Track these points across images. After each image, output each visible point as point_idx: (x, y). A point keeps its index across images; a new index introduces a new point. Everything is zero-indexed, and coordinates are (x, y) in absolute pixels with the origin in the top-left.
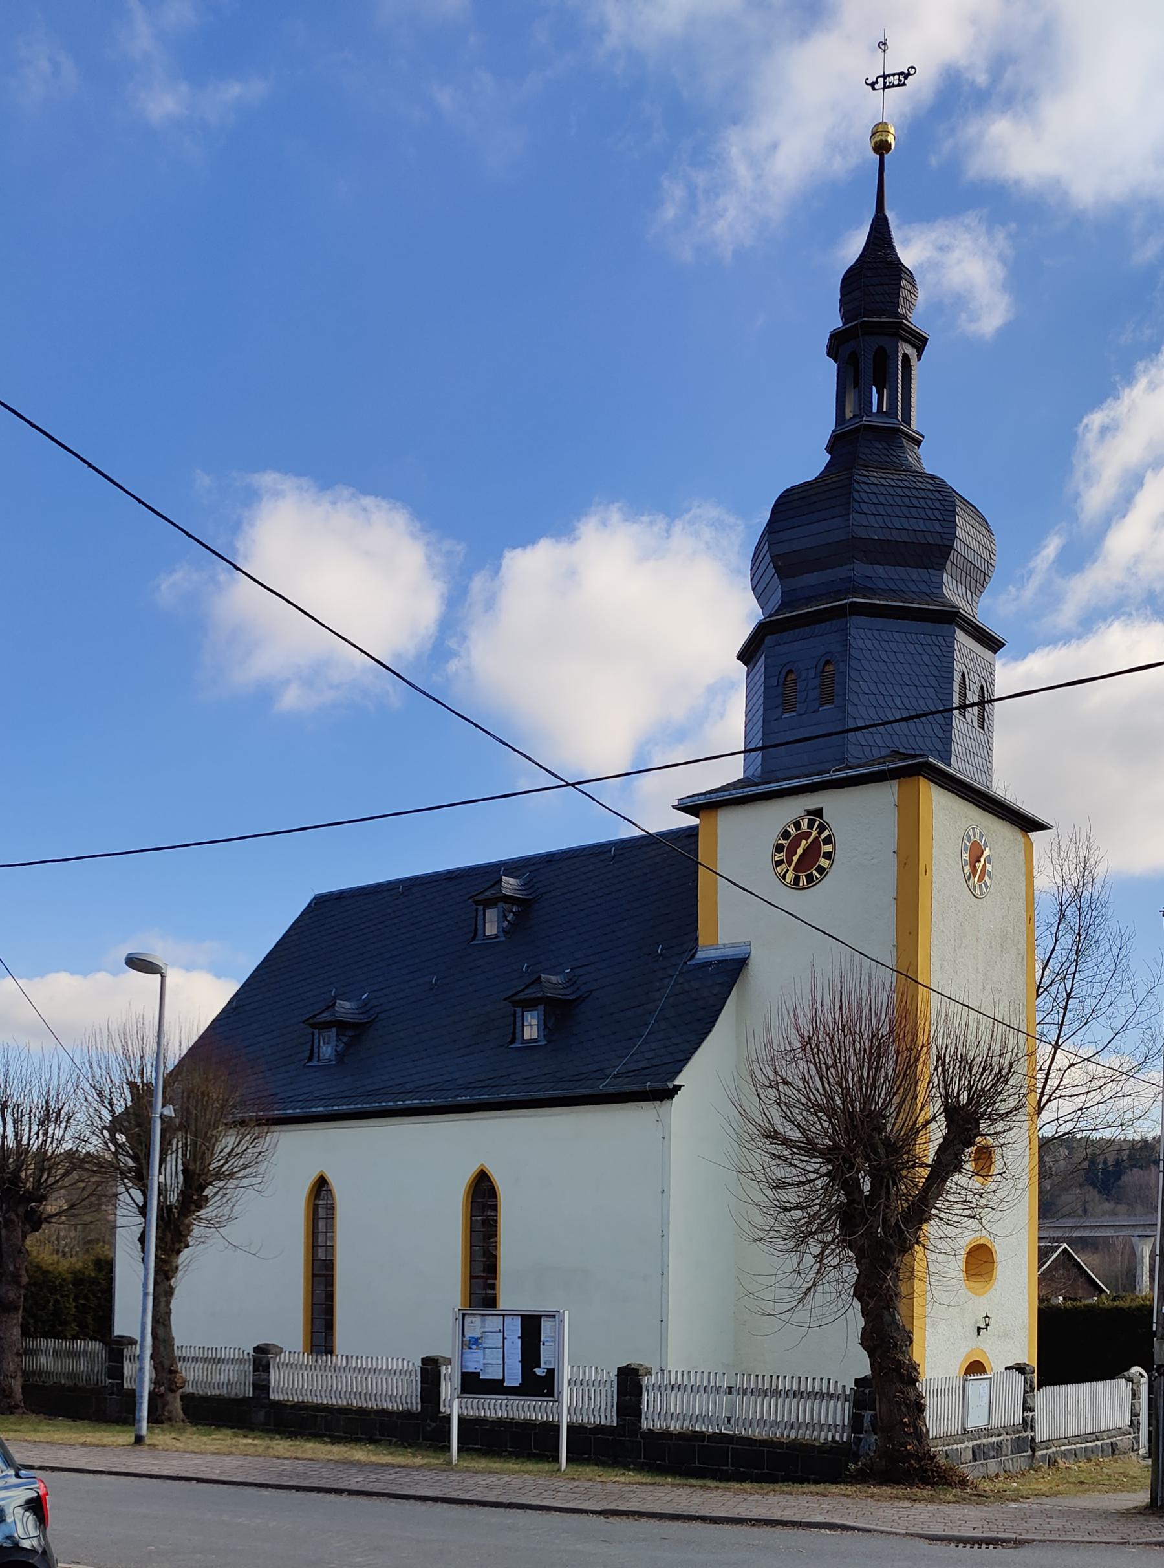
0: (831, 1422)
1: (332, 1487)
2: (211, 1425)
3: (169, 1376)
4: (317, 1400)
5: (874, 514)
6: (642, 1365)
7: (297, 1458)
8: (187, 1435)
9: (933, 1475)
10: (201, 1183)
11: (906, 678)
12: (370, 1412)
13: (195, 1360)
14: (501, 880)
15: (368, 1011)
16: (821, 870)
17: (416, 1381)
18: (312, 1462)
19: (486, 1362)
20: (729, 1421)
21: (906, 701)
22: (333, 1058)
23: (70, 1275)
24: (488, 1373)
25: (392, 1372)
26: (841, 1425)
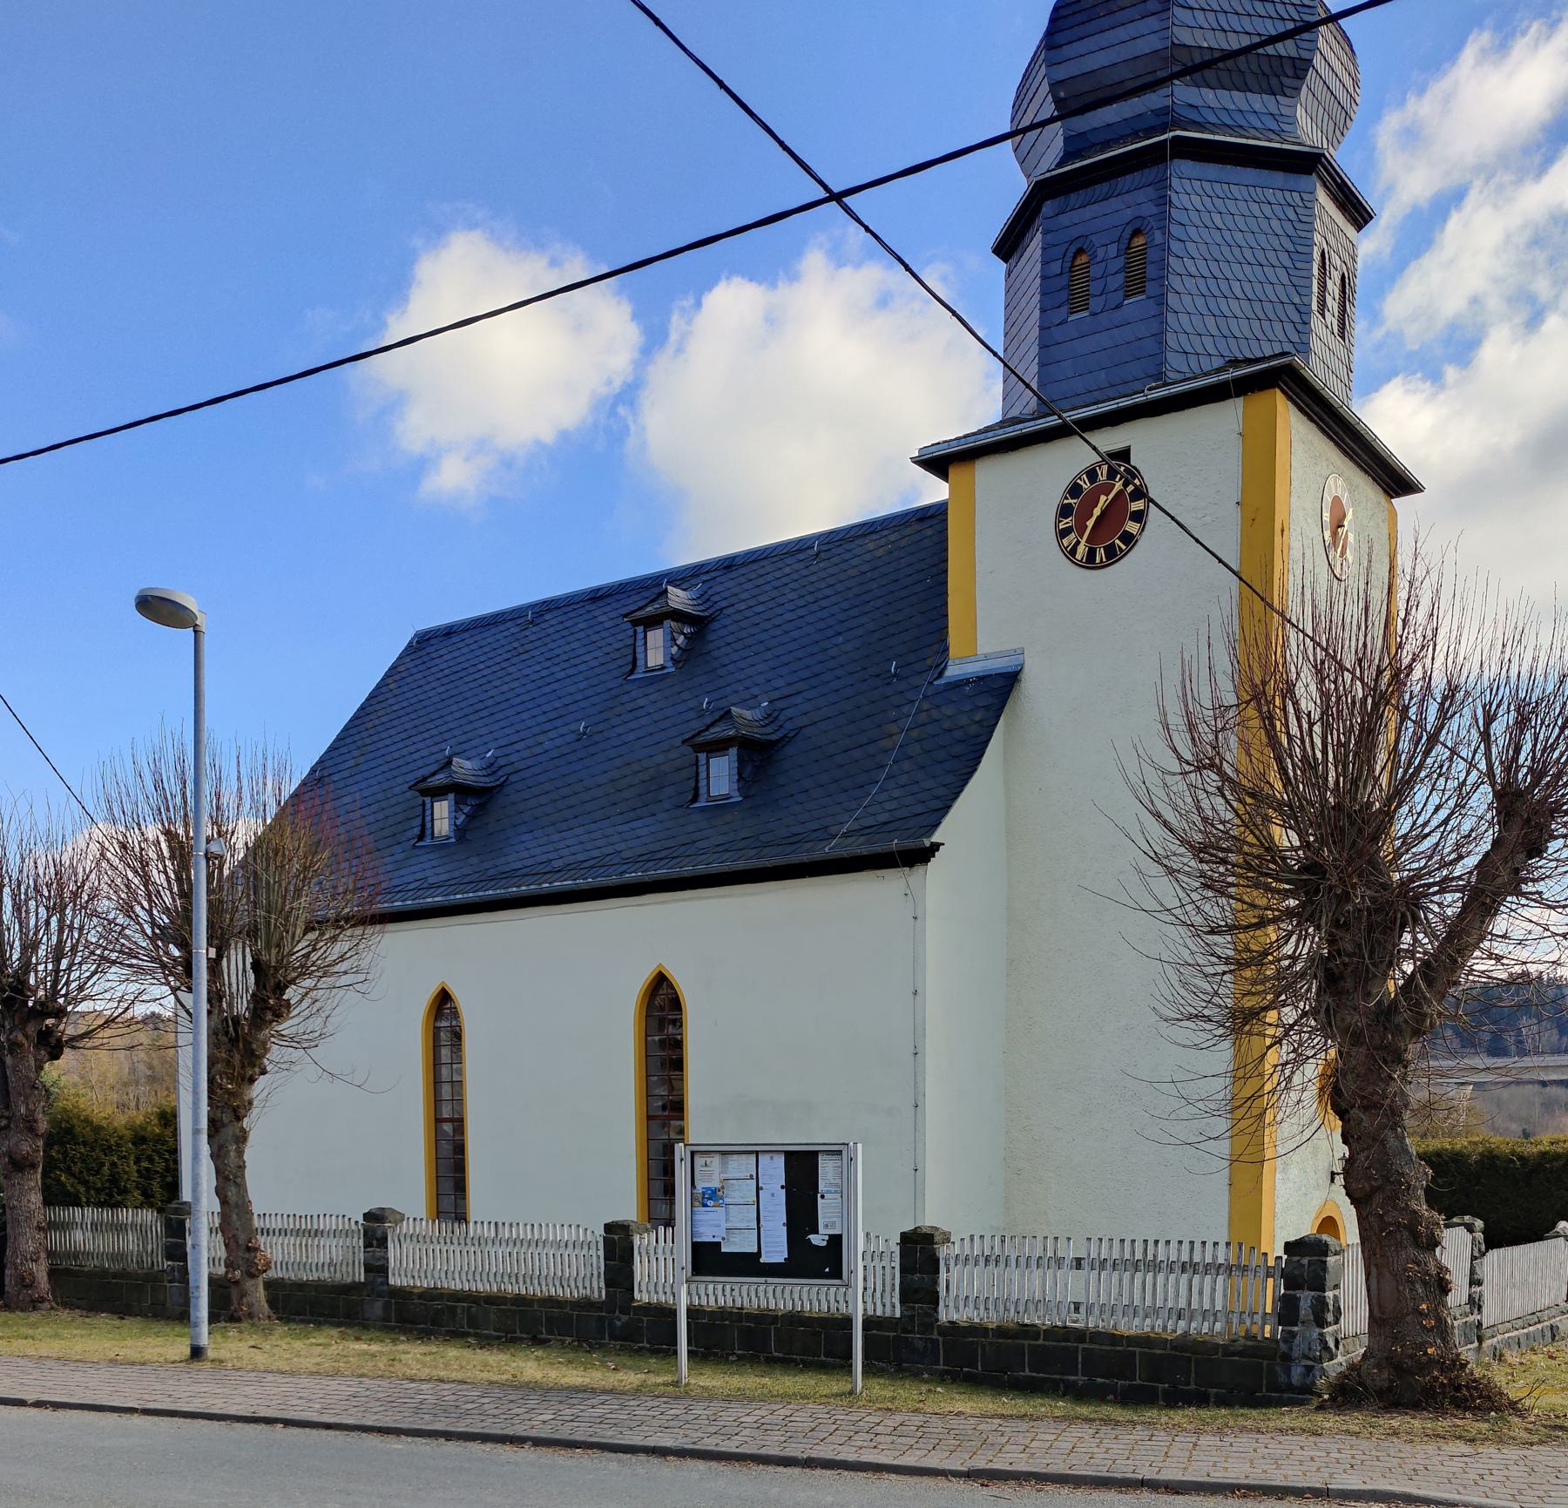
0: (1206, 1306)
1: (504, 1432)
2: (309, 1322)
3: (247, 1256)
4: (456, 1285)
5: (1203, 9)
6: (937, 1229)
7: (442, 1381)
8: (273, 1340)
9: (1471, 1395)
10: (280, 981)
11: (1248, 254)
12: (533, 1300)
13: (283, 1232)
14: (666, 591)
15: (494, 772)
17: (598, 1257)
18: (465, 1386)
19: (730, 1225)
20: (1077, 1309)
21: (1247, 287)
22: (452, 835)
23: (127, 1132)
24: (734, 1243)
25: (563, 1244)
26: (1260, 1312)
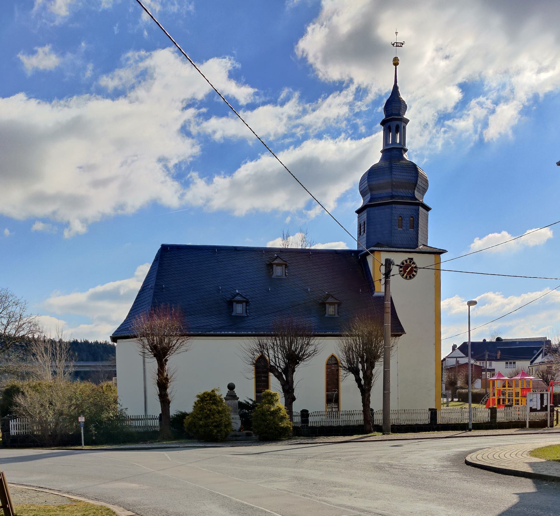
16: (414, 275)
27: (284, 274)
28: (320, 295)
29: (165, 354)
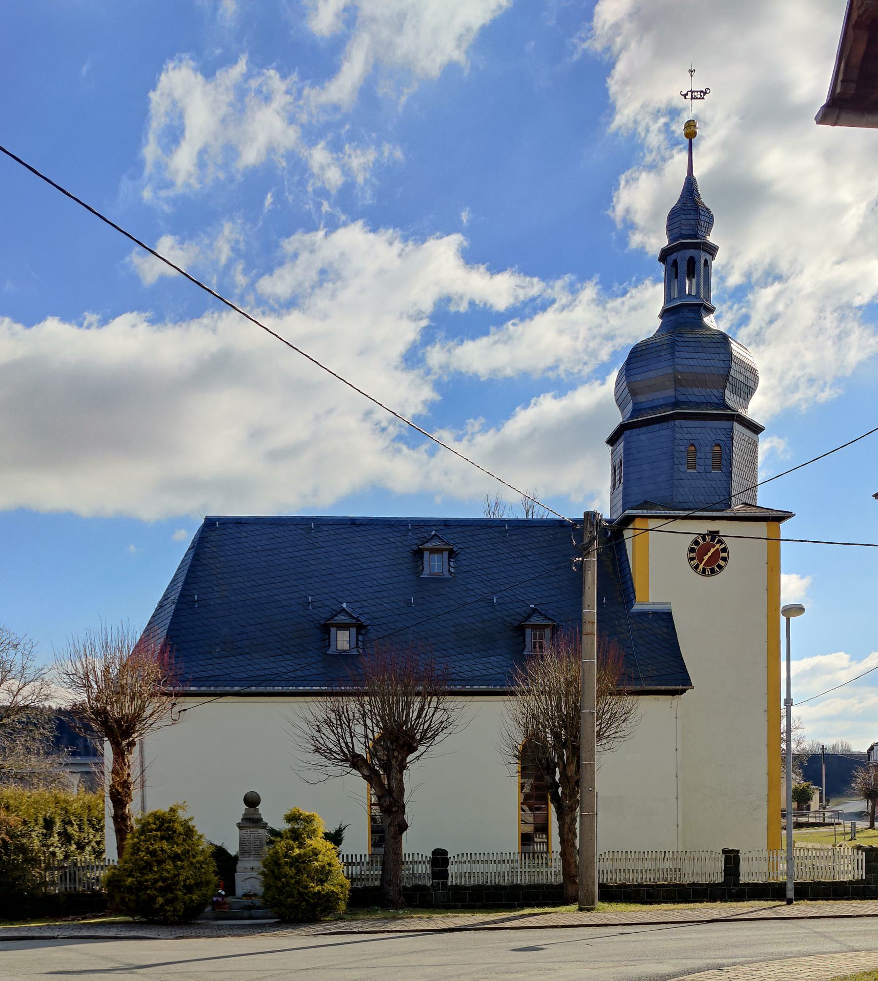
16: (692, 559)
27: (446, 570)
28: (518, 610)
29: (127, 733)
